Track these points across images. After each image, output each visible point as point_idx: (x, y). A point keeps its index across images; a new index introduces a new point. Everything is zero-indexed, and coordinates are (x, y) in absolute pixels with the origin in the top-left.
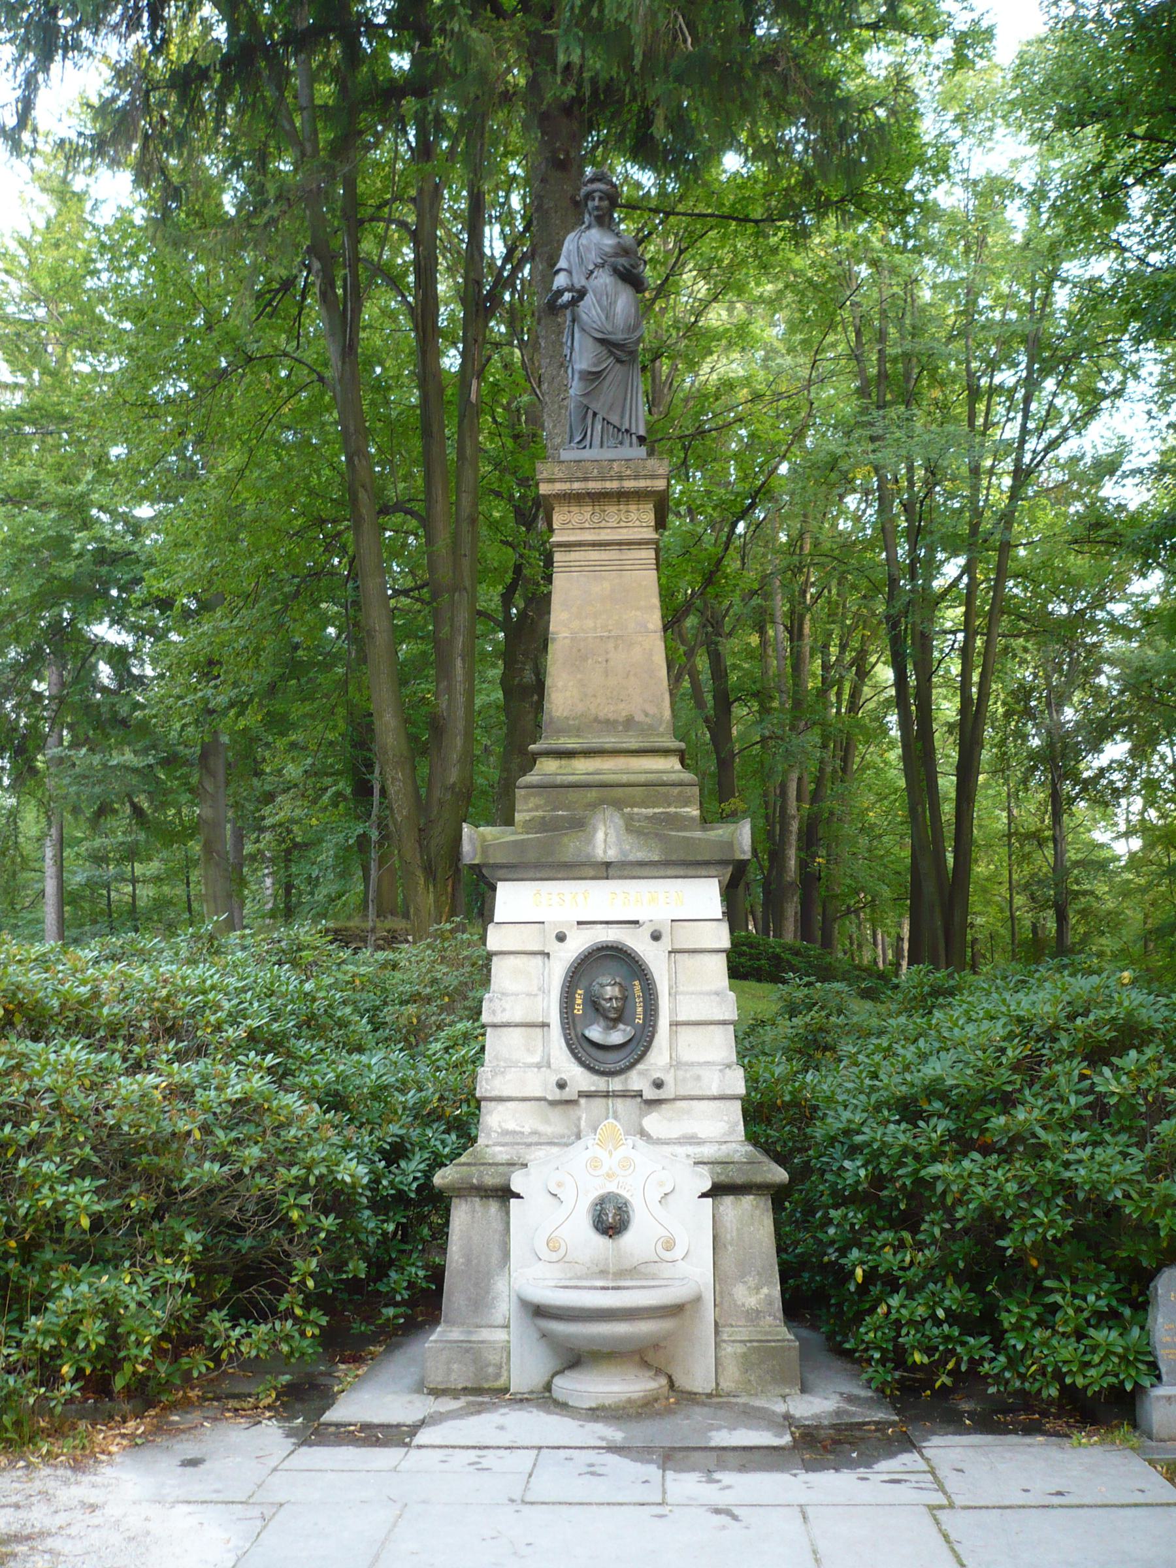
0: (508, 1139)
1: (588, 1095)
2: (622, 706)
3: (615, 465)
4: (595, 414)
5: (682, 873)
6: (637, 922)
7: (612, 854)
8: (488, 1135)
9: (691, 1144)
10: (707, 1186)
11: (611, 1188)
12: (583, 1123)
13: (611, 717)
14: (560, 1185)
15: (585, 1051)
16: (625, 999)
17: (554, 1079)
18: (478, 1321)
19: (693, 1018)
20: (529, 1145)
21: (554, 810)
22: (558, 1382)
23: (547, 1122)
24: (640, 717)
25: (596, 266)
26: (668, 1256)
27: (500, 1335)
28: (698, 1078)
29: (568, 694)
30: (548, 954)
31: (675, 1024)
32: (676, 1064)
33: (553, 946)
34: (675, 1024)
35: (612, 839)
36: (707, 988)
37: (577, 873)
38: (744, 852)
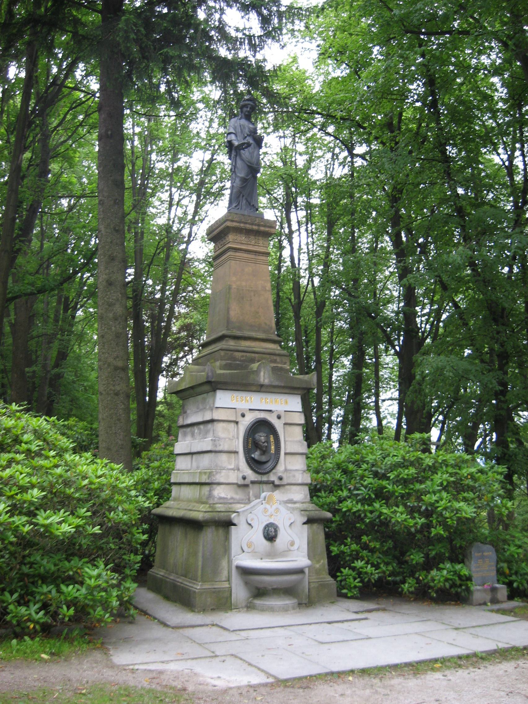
0: (221, 501)
1: (253, 482)
6: (270, 411)
8: (213, 499)
10: (305, 519)
11: (272, 521)
14: (252, 520)
17: (241, 475)
20: (231, 503)
23: (237, 493)
26: (292, 548)
27: (226, 585)
28: (294, 476)
31: (286, 454)
32: (286, 470)
33: (240, 419)
34: (286, 454)
35: (266, 376)
36: (296, 439)
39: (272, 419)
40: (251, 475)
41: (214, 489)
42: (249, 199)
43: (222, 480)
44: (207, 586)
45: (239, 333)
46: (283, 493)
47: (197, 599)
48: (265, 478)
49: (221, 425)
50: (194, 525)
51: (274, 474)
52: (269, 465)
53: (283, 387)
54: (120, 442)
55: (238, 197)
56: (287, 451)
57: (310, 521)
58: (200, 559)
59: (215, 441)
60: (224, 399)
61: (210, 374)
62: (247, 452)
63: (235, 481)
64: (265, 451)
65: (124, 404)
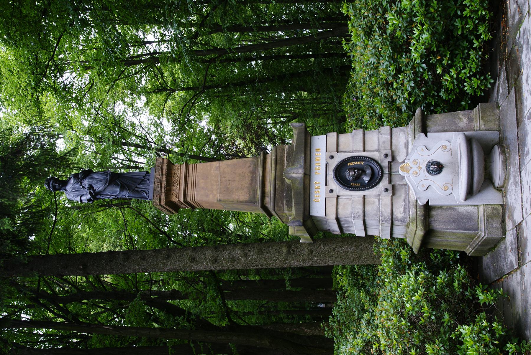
1: (390, 182)
2: (246, 175)
3: (157, 176)
4: (137, 187)
5: (309, 149)
6: (326, 165)
7: (301, 171)
8: (406, 218)
9: (408, 144)
10: (423, 135)
12: (401, 183)
13: (250, 178)
14: (423, 186)
15: (373, 182)
16: (355, 169)
18: (476, 218)
19: (362, 144)
20: (409, 202)
21: (284, 197)
22: (497, 184)
23: (400, 196)
24: (251, 169)
25: (81, 185)
26: (449, 148)
27: (481, 209)
28: (384, 142)
29: (240, 194)
30: (338, 196)
31: (364, 151)
32: (378, 150)
33: (334, 194)
34: (364, 151)
35: (296, 171)
37: (308, 186)
38: (302, 125)
39: (334, 164)
40: (384, 183)
41: (397, 217)
42: (139, 181)
43: (389, 211)
44: (482, 226)
45: (259, 192)
46: (399, 152)
47: (494, 236)
48: (386, 171)
49: (340, 211)
50: (429, 233)
51: (382, 162)
52: (377, 168)
53: (305, 154)
54: (353, 248)
55: (138, 191)
56: (362, 149)
57: (425, 130)
58: (458, 231)
59: (354, 217)
60: (318, 209)
61: (297, 224)
62: (364, 187)
63: (390, 198)
64: (362, 170)
65: (320, 244)
